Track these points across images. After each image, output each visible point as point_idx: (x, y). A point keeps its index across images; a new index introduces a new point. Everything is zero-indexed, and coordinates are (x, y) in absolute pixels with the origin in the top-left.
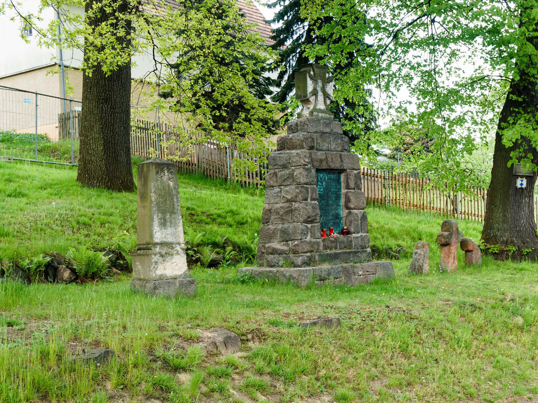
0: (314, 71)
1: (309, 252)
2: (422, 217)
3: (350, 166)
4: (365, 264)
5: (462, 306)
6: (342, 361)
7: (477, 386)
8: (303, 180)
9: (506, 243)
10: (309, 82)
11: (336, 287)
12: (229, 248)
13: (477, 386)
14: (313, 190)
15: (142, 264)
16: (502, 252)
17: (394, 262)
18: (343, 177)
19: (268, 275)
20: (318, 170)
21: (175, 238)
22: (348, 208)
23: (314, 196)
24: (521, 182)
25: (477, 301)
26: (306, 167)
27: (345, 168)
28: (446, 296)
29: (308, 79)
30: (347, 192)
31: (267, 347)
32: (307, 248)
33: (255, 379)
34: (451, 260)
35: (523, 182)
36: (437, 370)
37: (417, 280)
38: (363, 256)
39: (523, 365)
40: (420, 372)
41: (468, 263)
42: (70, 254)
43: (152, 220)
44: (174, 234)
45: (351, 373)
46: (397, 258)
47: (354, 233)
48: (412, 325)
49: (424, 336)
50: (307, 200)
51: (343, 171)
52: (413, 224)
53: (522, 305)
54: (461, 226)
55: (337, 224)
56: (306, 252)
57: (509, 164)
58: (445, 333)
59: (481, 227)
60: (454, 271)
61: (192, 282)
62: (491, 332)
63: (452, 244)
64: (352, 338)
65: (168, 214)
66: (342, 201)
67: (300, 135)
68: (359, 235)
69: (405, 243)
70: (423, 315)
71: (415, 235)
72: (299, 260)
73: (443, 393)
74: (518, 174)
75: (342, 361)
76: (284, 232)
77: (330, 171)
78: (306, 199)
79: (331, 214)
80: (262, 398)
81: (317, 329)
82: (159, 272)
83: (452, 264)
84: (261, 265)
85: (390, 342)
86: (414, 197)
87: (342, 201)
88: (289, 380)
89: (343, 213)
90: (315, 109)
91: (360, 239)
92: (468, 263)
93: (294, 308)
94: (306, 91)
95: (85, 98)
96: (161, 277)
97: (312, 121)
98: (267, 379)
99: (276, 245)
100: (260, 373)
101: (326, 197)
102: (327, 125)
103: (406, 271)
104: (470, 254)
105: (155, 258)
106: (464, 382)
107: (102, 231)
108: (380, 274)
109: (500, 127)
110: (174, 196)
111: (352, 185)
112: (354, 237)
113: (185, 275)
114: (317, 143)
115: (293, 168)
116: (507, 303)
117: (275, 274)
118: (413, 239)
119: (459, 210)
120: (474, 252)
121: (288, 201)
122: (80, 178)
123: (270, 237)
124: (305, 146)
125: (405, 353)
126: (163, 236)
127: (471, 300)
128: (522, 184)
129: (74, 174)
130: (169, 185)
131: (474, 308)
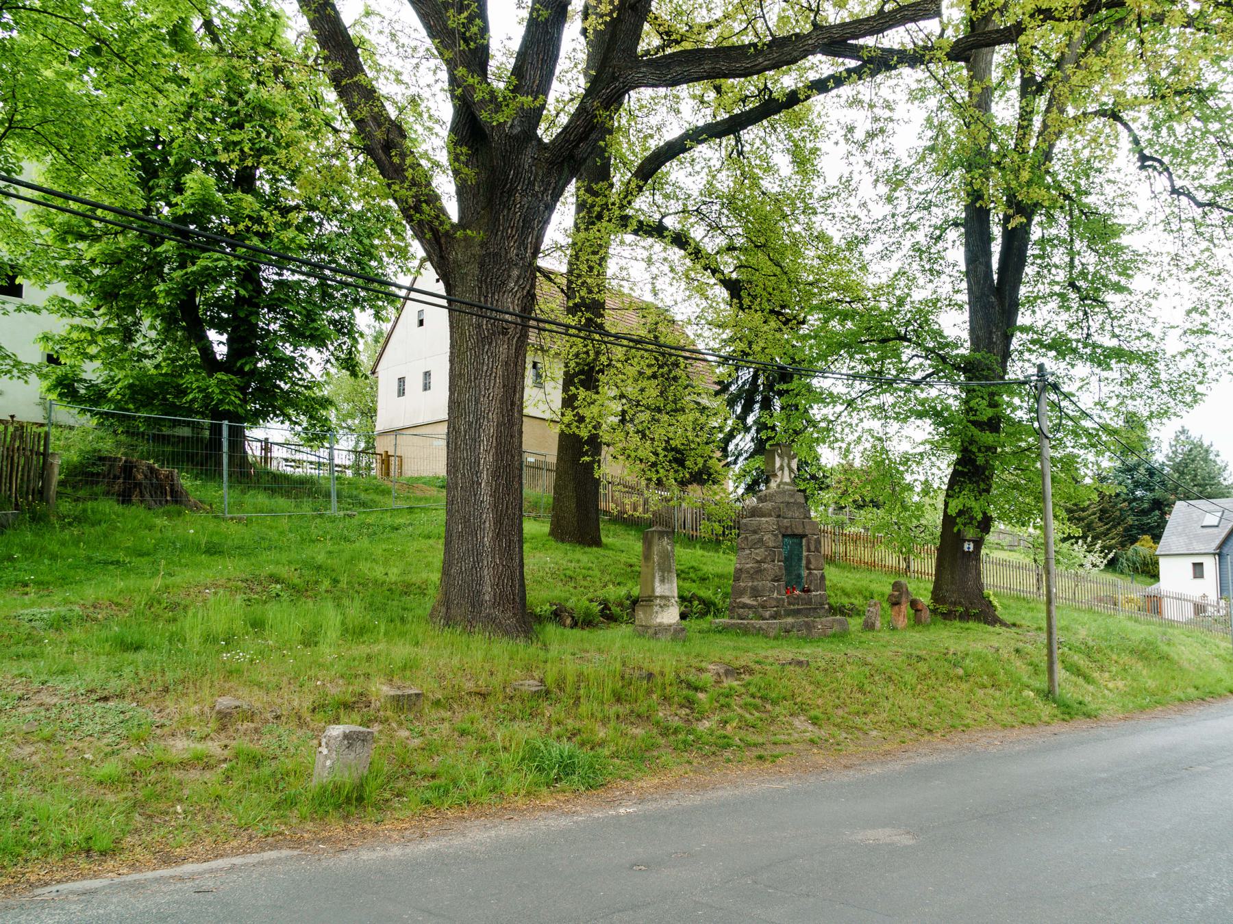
2: (873, 576)
4: (824, 619)
5: (910, 656)
6: (813, 692)
7: (920, 719)
8: (771, 544)
9: (955, 604)
10: (777, 459)
11: (799, 638)
12: (696, 603)
13: (920, 719)
14: (780, 553)
15: (645, 613)
16: (950, 612)
17: (849, 620)
18: (804, 541)
19: (739, 626)
20: (784, 536)
22: (808, 568)
25: (923, 653)
28: (895, 648)
31: (756, 678)
32: (774, 603)
33: (749, 700)
34: (901, 618)
36: (887, 705)
37: (870, 635)
38: (822, 612)
39: (959, 706)
40: (874, 705)
41: (918, 621)
42: (570, 604)
43: (654, 577)
44: (670, 589)
45: (820, 702)
46: (850, 616)
48: (867, 670)
49: (877, 678)
51: (805, 536)
52: (865, 583)
53: (963, 658)
54: (911, 587)
55: (799, 583)
57: (955, 530)
58: (894, 677)
59: (931, 587)
60: (905, 629)
61: (683, 630)
62: (933, 678)
64: (819, 676)
66: (804, 562)
67: (768, 505)
69: (858, 601)
70: (876, 661)
71: (868, 594)
72: (767, 614)
73: (892, 722)
75: (813, 692)
76: (754, 589)
77: (794, 536)
81: (792, 668)
82: (658, 620)
83: (902, 622)
84: (732, 618)
85: (849, 681)
86: (864, 553)
87: (804, 562)
88: (775, 703)
89: (805, 573)
90: (781, 482)
92: (918, 621)
93: (769, 653)
95: (560, 458)
96: (660, 625)
97: (780, 493)
98: (758, 701)
99: (746, 600)
100: (753, 696)
102: (792, 496)
103: (859, 627)
105: (656, 609)
106: (909, 715)
107: (585, 583)
108: (836, 628)
109: (948, 496)
111: (812, 548)
113: (678, 624)
115: (96, 224)
116: (950, 656)
117: (746, 626)
118: (865, 598)
119: (912, 569)
121: (758, 562)
122: (553, 533)
123: (741, 593)
125: (861, 689)
127: (918, 652)
129: (546, 528)
131: (920, 658)
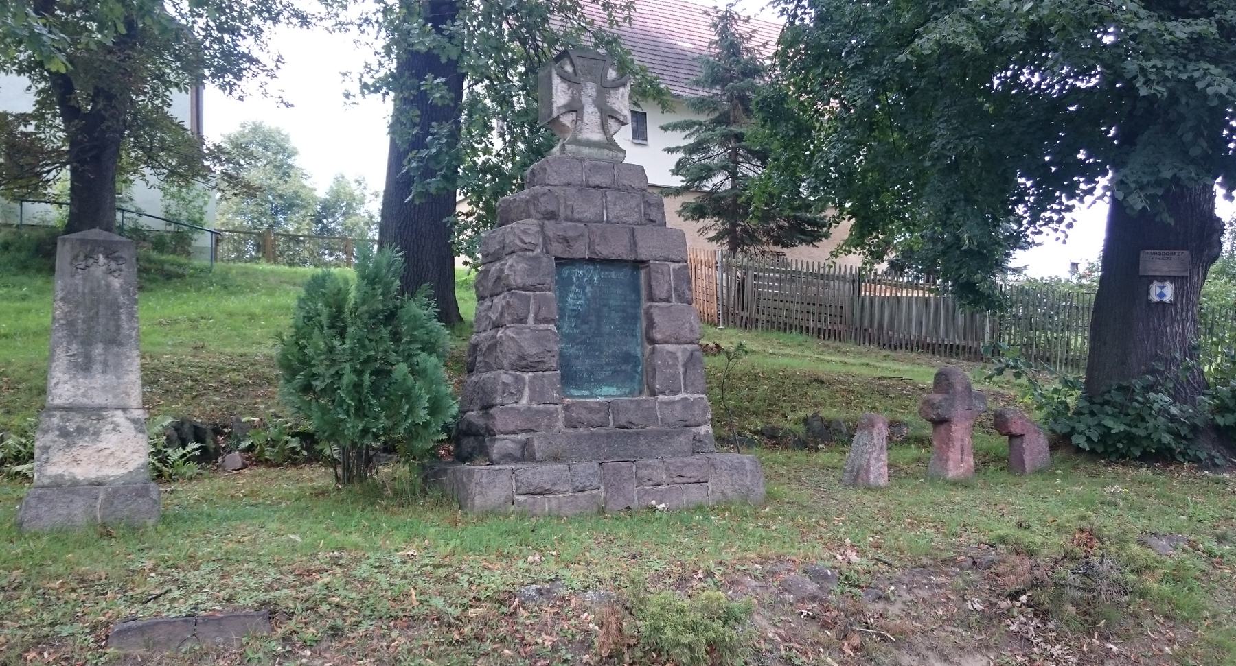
0: (573, 65)
1: (522, 431)
3: (658, 253)
18: (643, 274)
21: (115, 396)
23: (544, 313)
24: (1158, 291)
26: (531, 254)
27: (643, 257)
29: (556, 81)
30: (650, 307)
35: (1164, 291)
47: (663, 393)
50: (526, 323)
56: (514, 433)
63: (955, 420)
65: (100, 346)
68: (678, 397)
74: (1151, 273)
78: (522, 320)
79: (607, 352)
80: (1176, 664)
91: (678, 407)
94: (551, 104)
101: (593, 318)
104: (1018, 441)
110: (120, 308)
112: (662, 403)
114: (566, 206)
120: (1026, 439)
124: (533, 212)
126: (79, 392)
128: (1162, 295)
130: (108, 286)
